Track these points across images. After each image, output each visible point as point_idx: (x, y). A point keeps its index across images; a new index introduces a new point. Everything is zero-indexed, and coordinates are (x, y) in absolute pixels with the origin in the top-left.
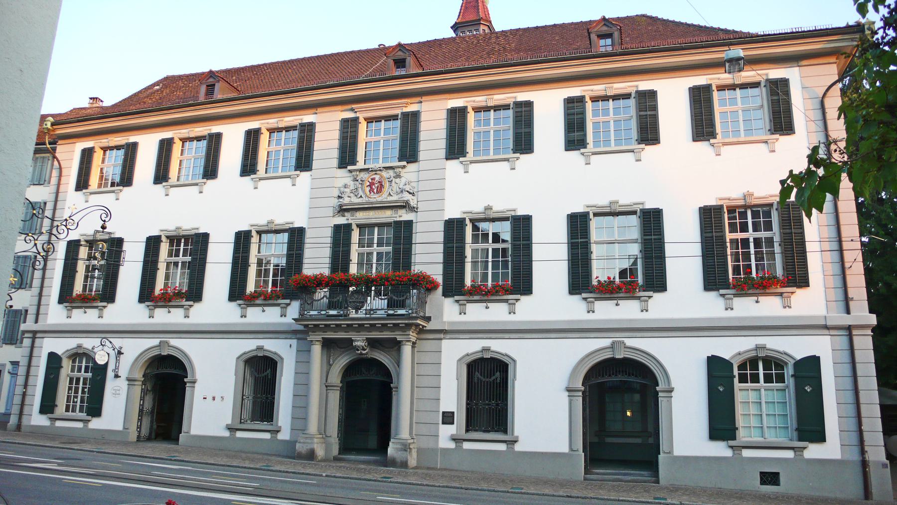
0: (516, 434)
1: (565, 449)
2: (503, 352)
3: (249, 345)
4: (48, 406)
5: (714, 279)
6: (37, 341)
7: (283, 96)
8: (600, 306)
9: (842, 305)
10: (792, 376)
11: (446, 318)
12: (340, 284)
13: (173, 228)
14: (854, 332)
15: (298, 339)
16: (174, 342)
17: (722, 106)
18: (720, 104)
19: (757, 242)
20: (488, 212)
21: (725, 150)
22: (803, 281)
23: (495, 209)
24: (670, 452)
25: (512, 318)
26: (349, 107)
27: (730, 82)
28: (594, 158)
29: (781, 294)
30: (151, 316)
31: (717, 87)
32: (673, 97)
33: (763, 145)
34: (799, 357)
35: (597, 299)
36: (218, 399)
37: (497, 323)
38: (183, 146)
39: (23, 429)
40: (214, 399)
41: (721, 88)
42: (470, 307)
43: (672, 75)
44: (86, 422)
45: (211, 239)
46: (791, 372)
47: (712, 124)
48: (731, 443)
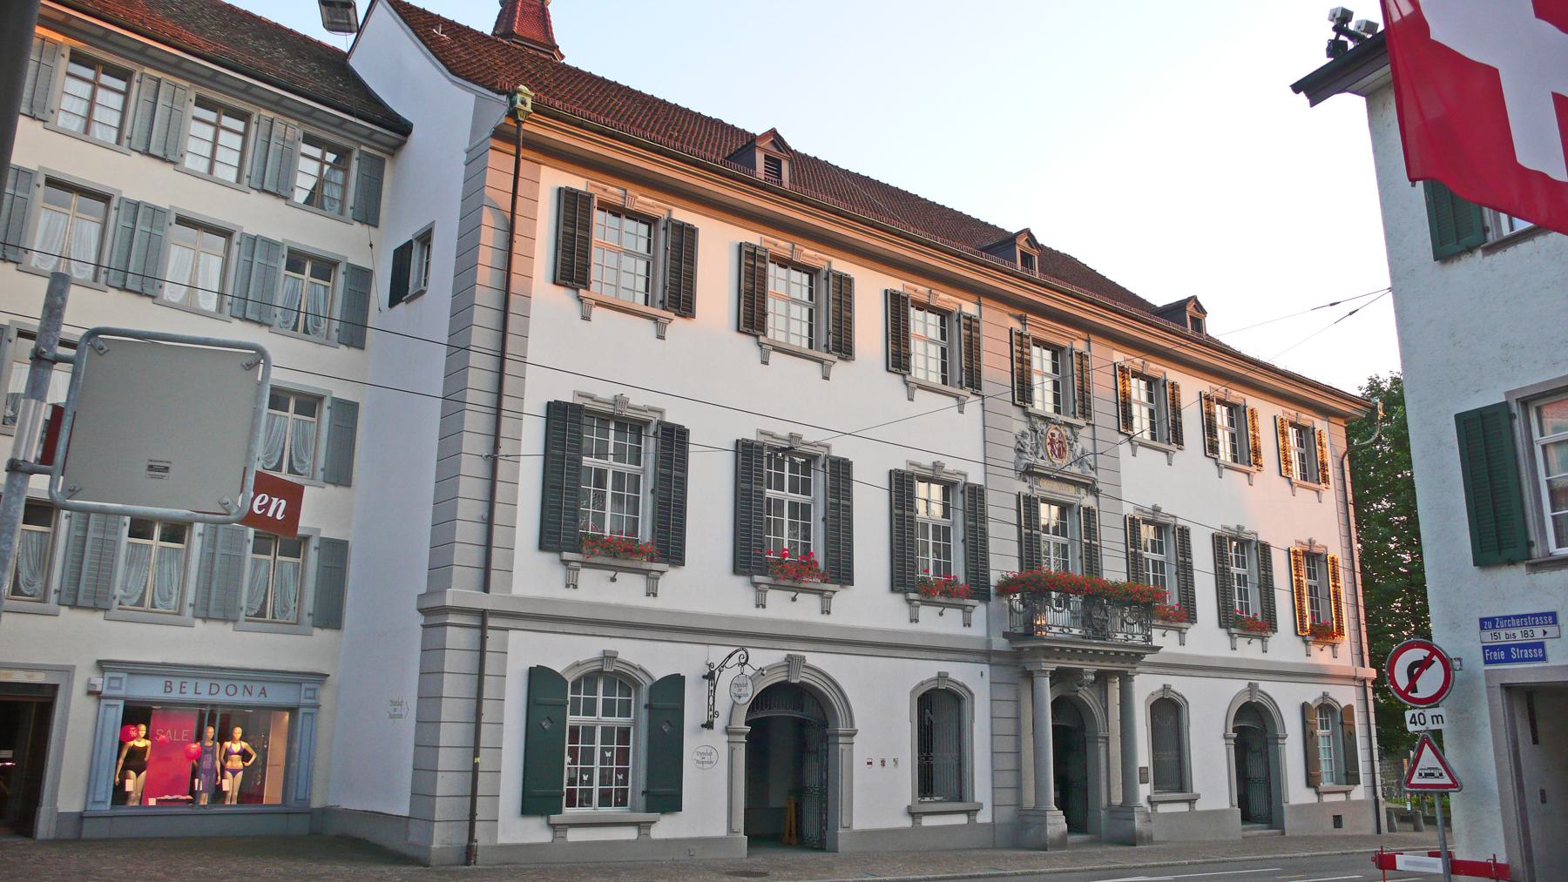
0: (977, 799)
1: (721, 831)
2: (635, 662)
3: (925, 671)
4: (1312, 781)
5: (749, 557)
7: (967, 264)
8: (927, 612)
9: (476, 576)
11: (517, 590)
12: (1032, 587)
14: (491, 622)
19: (618, 476)
22: (675, 556)
25: (650, 603)
26: (1019, 313)
28: (597, 312)
29: (646, 572)
30: (914, 620)
34: (658, 676)
35: (586, 565)
36: (889, 763)
37: (1214, 658)
38: (811, 283)
40: (883, 763)
42: (586, 576)
43: (879, 266)
44: (1347, 793)
45: (692, 438)
46: (644, 699)
47: (585, 267)
48: (555, 818)
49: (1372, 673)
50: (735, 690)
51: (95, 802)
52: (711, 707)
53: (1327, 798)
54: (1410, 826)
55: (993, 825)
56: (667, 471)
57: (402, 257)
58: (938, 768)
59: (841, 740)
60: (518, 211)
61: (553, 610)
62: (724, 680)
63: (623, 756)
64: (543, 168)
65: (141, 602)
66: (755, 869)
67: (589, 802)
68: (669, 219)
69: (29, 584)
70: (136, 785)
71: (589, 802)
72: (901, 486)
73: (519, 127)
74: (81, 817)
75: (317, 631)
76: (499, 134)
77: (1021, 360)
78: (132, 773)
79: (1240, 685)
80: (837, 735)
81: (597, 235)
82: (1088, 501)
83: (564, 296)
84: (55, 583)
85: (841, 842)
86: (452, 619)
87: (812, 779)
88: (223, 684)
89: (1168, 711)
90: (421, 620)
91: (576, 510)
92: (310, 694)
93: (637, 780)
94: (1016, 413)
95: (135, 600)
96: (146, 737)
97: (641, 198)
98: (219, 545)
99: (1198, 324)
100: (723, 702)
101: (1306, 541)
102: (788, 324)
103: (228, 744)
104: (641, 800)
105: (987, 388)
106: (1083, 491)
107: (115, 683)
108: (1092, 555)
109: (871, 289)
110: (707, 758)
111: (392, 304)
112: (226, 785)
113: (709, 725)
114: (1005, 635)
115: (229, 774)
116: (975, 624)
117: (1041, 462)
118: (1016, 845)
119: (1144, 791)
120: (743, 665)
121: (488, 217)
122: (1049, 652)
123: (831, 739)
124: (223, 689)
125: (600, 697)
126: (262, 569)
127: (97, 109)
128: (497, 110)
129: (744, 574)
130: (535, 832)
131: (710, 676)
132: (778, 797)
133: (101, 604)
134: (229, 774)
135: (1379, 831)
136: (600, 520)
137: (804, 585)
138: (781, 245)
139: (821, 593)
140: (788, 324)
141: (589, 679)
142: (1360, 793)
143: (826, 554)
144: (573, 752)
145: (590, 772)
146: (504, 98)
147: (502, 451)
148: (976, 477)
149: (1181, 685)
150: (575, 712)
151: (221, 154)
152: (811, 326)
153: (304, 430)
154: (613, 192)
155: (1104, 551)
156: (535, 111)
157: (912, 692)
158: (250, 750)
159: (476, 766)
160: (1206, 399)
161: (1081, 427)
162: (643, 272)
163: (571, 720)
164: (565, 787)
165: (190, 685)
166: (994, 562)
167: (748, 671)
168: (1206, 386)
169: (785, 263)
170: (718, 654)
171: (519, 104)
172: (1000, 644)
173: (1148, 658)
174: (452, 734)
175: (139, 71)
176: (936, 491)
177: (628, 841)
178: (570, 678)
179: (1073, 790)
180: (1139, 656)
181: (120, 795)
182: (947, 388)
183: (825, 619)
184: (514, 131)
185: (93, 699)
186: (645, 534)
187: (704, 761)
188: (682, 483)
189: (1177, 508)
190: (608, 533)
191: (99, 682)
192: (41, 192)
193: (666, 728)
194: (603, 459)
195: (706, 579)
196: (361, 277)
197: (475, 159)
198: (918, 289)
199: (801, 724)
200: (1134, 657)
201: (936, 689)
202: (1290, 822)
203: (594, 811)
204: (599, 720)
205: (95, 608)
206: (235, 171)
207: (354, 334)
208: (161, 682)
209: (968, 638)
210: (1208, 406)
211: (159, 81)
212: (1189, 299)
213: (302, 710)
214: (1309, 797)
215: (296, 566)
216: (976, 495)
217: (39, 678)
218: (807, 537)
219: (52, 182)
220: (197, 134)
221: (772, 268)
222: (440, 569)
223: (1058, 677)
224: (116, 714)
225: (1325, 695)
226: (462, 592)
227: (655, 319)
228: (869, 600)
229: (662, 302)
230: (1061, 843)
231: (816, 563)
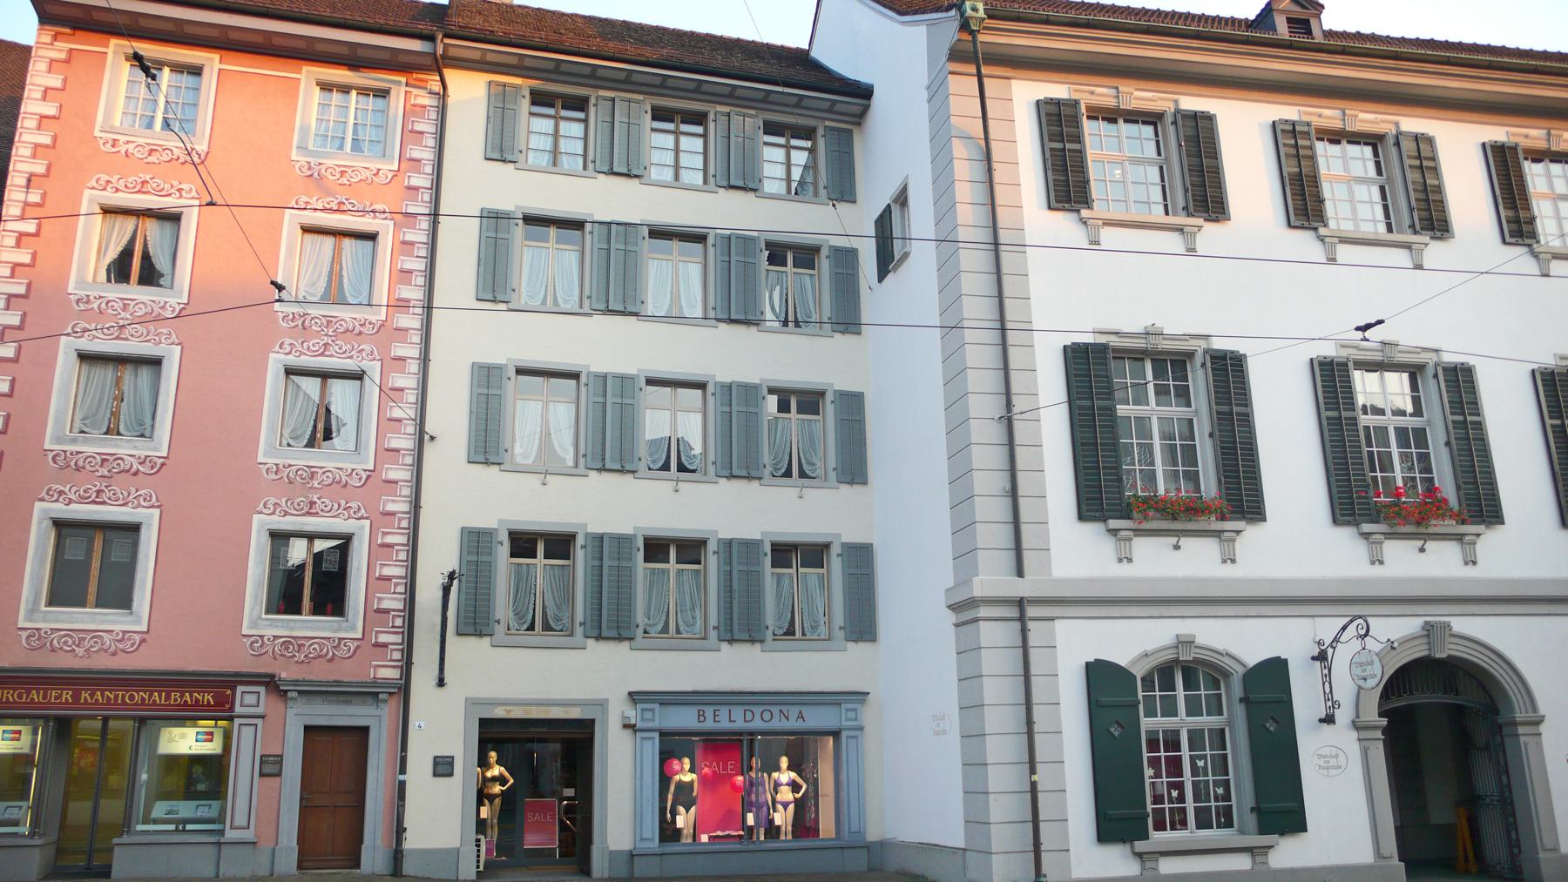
2: (1220, 646)
8: (1144, 548)
9: (1008, 558)
10: (1241, 700)
11: (1059, 571)
13: (1138, 328)
14: (1031, 611)
17: (1104, 147)
18: (1098, 140)
20: (1152, 339)
24: (1556, 849)
25: (1229, 571)
27: (1337, 124)
31: (1089, 108)
32: (1461, 150)
33: (1176, 235)
34: (1252, 661)
35: (1139, 532)
38: (1376, 154)
41: (1096, 113)
46: (1238, 691)
47: (1084, 184)
48: (1140, 846)
50: (1358, 671)
51: (642, 839)
56: (1225, 408)
57: (884, 224)
59: (1521, 730)
60: (992, 135)
61: (1120, 593)
62: (1342, 658)
63: (1222, 765)
65: (665, 629)
67: (1184, 824)
68: (1178, 111)
69: (558, 620)
70: (686, 822)
71: (1184, 824)
72: (1331, 379)
73: (974, 41)
74: (632, 855)
75: (851, 645)
76: (956, 55)
78: (681, 809)
80: (1515, 724)
81: (1091, 152)
83: (1063, 225)
84: (579, 617)
86: (984, 612)
87: (1486, 783)
88: (758, 710)
90: (952, 618)
91: (1117, 468)
92: (851, 715)
93: (1243, 797)
95: (660, 627)
96: (692, 770)
97: (1137, 94)
98: (735, 562)
102: (1354, 210)
103: (775, 775)
104: (1251, 820)
107: (648, 715)
110: (1333, 762)
111: (880, 280)
112: (778, 819)
113: (1329, 719)
115: (780, 807)
121: (959, 149)
123: (1505, 730)
124: (758, 716)
126: (786, 581)
127: (562, 141)
128: (948, 26)
129: (1348, 523)
131: (1321, 657)
132: (1441, 811)
133: (625, 634)
134: (780, 807)
136: (1150, 477)
137: (1432, 530)
138: (1327, 114)
139: (1459, 538)
140: (1354, 210)
141: (1164, 674)
143: (1458, 488)
144: (1155, 762)
145: (1180, 786)
146: (953, 12)
147: (1015, 410)
150: (1151, 713)
151: (685, 160)
152: (1386, 207)
153: (810, 429)
154: (1101, 93)
156: (990, 17)
158: (799, 780)
159: (1034, 785)
162: (1160, 198)
163: (1146, 723)
164: (1150, 807)
165: (723, 712)
169: (1335, 137)
170: (1327, 628)
171: (969, 12)
174: (1002, 749)
175: (593, 95)
177: (1239, 872)
178: (1139, 672)
181: (669, 832)
182: (1171, 220)
183: (1470, 572)
184: (970, 47)
185: (629, 732)
186: (1209, 486)
187: (1329, 765)
188: (1247, 420)
190: (1161, 492)
191: (632, 714)
192: (519, 229)
193: (1272, 727)
194: (1146, 411)
195: (1297, 530)
196: (846, 259)
197: (937, 93)
199: (1458, 712)
205: (620, 639)
206: (701, 174)
207: (847, 320)
208: (693, 710)
211: (613, 100)
213: (844, 734)
215: (821, 578)
217: (575, 713)
218: (1428, 470)
219: (529, 220)
220: (659, 144)
221: (1320, 147)
222: (965, 556)
224: (652, 748)
226: (992, 579)
227: (1180, 229)
229: (1186, 208)
231: (1445, 501)
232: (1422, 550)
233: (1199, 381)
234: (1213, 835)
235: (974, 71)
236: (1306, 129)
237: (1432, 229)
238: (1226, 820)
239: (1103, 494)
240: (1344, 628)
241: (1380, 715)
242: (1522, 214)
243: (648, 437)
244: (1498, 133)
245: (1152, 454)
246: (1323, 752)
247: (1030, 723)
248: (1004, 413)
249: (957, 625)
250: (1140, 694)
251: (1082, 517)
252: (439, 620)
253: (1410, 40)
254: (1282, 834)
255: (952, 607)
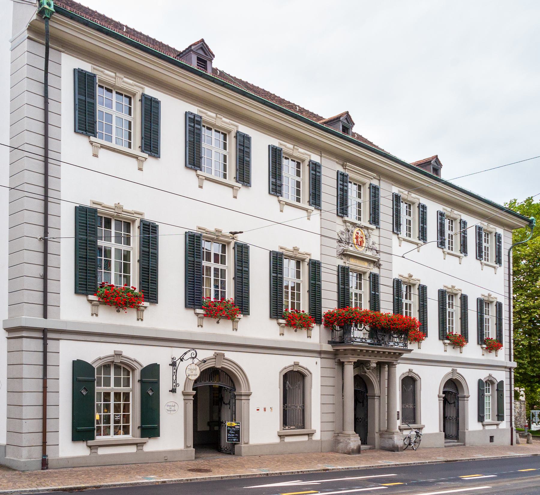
2: (132, 357)
3: (286, 362)
4: (481, 419)
6: (51, 345)
7: (505, 213)
10: (139, 381)
14: (50, 335)
15: (321, 358)
16: (229, 355)
20: (295, 252)
21: (102, 152)
23: (300, 251)
25: (234, 333)
33: (305, 212)
34: (145, 365)
36: (268, 409)
38: (225, 139)
39: (50, 464)
40: (265, 409)
44: (497, 425)
48: (90, 443)
49: (514, 364)
52: (175, 381)
53: (487, 428)
54: (525, 440)
55: (321, 441)
56: (147, 250)
58: (293, 414)
62: (182, 367)
64: (63, 54)
66: (202, 467)
72: (277, 260)
77: (342, 190)
79: (449, 370)
82: (375, 271)
83: (82, 142)
85: (243, 451)
89: (410, 382)
90: (6, 334)
94: (339, 220)
99: (437, 170)
100: (181, 380)
101: (406, 275)
104: (138, 432)
105: (323, 205)
106: (372, 265)
108: (375, 300)
109: (261, 144)
110: (173, 408)
113: (173, 391)
114: (329, 342)
116: (317, 336)
117: (351, 248)
118: (334, 450)
119: (399, 423)
120: (193, 358)
122: (354, 352)
125: (112, 376)
130: (81, 450)
131: (173, 364)
135: (512, 444)
142: (504, 425)
148: (316, 257)
149: (418, 370)
155: (323, 269)
157: (280, 372)
160: (441, 215)
161: (372, 229)
163: (97, 389)
166: (324, 303)
167: (196, 361)
168: (441, 208)
170: (178, 352)
172: (329, 348)
173: (405, 355)
176: (293, 263)
179: (362, 424)
180: (400, 354)
189: (422, 277)
195: (170, 311)
198: (287, 147)
200: (397, 355)
201: (292, 371)
202: (469, 439)
203: (112, 437)
204: (112, 388)
209: (461, 358)
210: (441, 219)
212: (433, 158)
214: (478, 427)
216: (315, 267)
223: (358, 365)
225: (490, 376)
226: (32, 318)
228: (258, 325)
230: (358, 451)
232: (218, 322)
233: (135, 234)
234: (122, 437)
235: (44, 42)
236: (199, 119)
237: (244, 181)
238: (126, 431)
239: (86, 282)
240: (185, 354)
241: (194, 389)
242: (278, 182)
243: (392, 312)
244: (276, 142)
245: (110, 265)
246: (169, 404)
247: (45, 387)
248: (42, 236)
249: (8, 338)
250: (96, 376)
251: (77, 292)
252: (28, 339)
253: (243, 82)
254: (149, 438)
255: (8, 330)
